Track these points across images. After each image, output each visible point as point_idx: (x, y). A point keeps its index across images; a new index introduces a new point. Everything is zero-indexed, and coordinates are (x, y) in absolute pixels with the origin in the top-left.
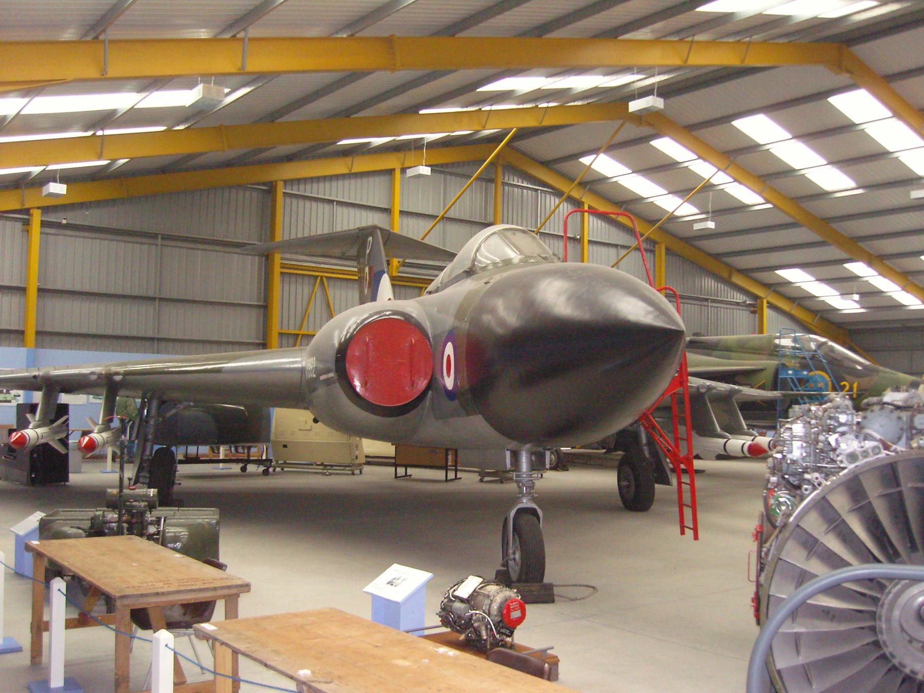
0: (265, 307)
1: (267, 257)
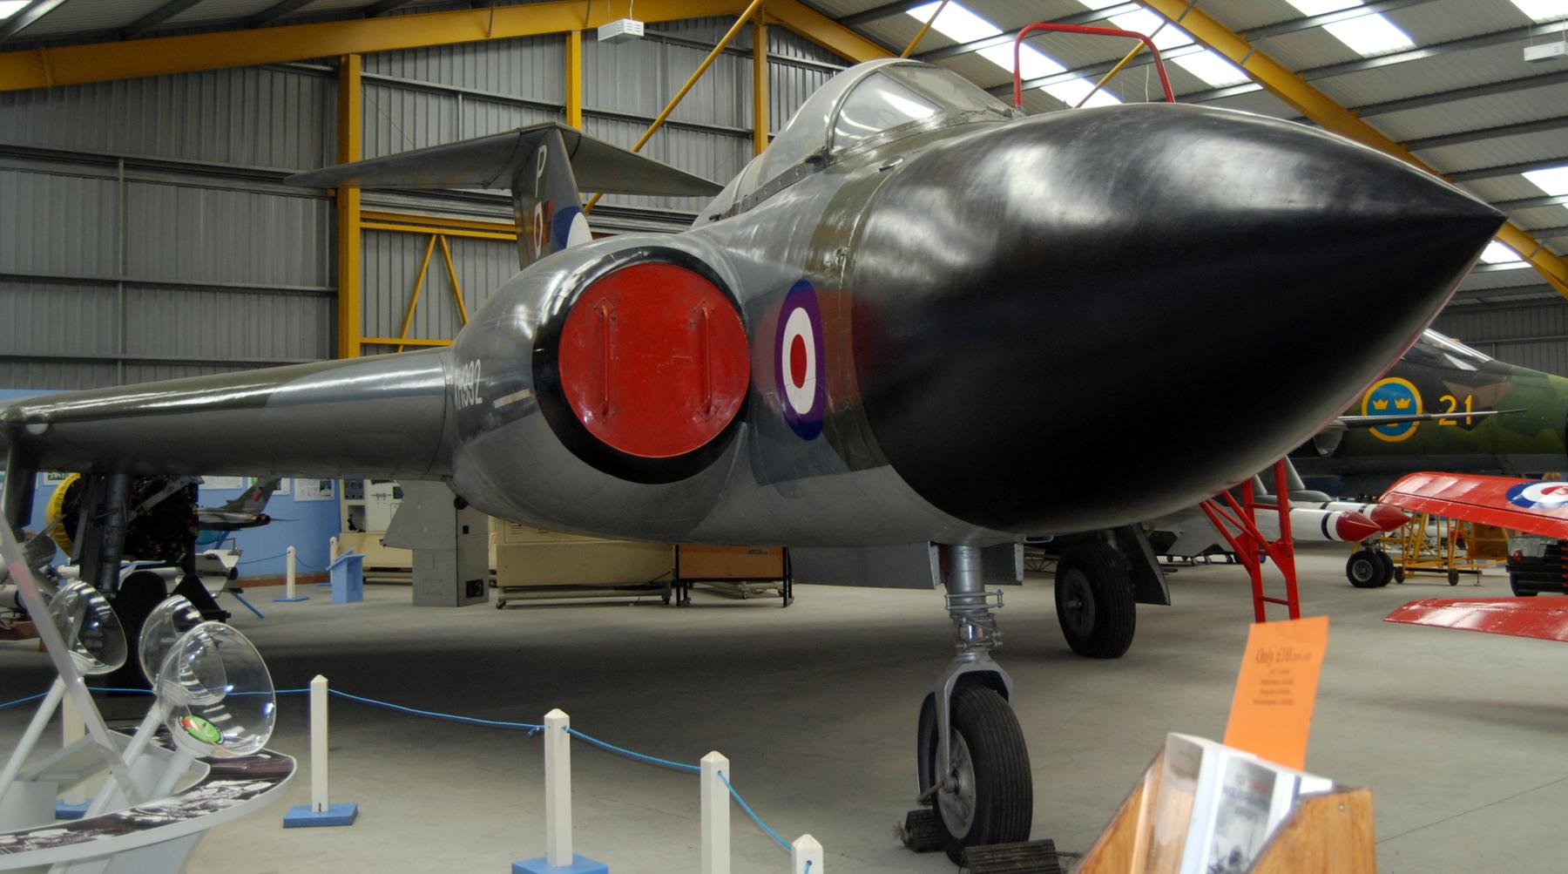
0: (332, 296)
1: (331, 197)
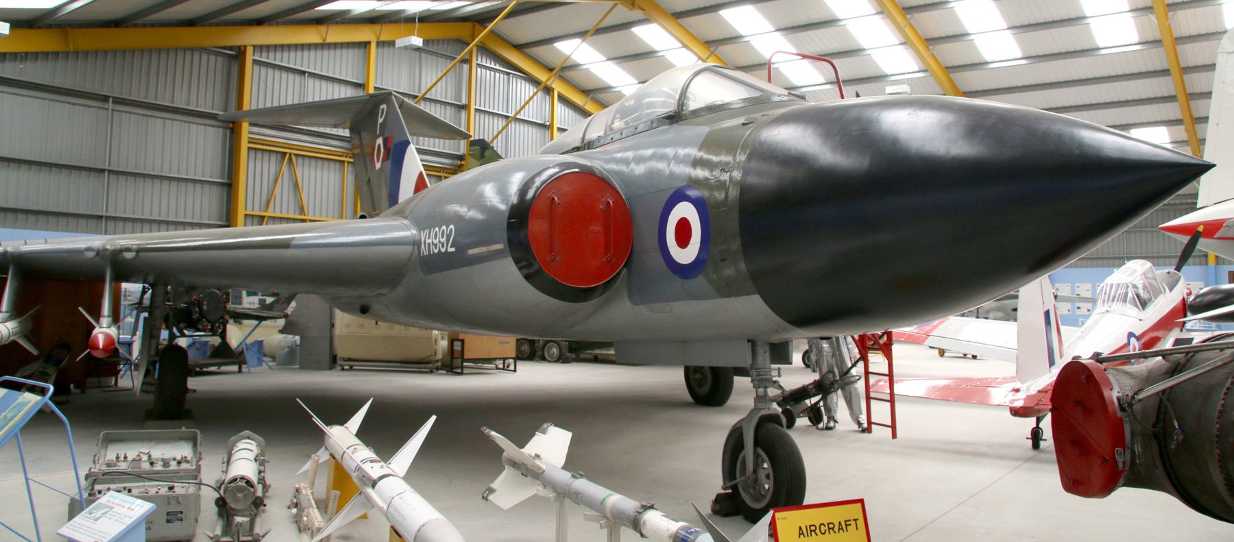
0: (229, 186)
1: (232, 128)
